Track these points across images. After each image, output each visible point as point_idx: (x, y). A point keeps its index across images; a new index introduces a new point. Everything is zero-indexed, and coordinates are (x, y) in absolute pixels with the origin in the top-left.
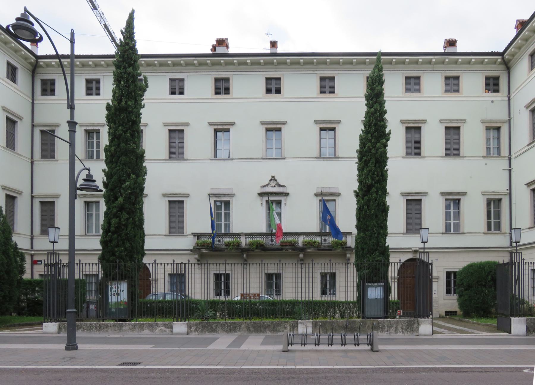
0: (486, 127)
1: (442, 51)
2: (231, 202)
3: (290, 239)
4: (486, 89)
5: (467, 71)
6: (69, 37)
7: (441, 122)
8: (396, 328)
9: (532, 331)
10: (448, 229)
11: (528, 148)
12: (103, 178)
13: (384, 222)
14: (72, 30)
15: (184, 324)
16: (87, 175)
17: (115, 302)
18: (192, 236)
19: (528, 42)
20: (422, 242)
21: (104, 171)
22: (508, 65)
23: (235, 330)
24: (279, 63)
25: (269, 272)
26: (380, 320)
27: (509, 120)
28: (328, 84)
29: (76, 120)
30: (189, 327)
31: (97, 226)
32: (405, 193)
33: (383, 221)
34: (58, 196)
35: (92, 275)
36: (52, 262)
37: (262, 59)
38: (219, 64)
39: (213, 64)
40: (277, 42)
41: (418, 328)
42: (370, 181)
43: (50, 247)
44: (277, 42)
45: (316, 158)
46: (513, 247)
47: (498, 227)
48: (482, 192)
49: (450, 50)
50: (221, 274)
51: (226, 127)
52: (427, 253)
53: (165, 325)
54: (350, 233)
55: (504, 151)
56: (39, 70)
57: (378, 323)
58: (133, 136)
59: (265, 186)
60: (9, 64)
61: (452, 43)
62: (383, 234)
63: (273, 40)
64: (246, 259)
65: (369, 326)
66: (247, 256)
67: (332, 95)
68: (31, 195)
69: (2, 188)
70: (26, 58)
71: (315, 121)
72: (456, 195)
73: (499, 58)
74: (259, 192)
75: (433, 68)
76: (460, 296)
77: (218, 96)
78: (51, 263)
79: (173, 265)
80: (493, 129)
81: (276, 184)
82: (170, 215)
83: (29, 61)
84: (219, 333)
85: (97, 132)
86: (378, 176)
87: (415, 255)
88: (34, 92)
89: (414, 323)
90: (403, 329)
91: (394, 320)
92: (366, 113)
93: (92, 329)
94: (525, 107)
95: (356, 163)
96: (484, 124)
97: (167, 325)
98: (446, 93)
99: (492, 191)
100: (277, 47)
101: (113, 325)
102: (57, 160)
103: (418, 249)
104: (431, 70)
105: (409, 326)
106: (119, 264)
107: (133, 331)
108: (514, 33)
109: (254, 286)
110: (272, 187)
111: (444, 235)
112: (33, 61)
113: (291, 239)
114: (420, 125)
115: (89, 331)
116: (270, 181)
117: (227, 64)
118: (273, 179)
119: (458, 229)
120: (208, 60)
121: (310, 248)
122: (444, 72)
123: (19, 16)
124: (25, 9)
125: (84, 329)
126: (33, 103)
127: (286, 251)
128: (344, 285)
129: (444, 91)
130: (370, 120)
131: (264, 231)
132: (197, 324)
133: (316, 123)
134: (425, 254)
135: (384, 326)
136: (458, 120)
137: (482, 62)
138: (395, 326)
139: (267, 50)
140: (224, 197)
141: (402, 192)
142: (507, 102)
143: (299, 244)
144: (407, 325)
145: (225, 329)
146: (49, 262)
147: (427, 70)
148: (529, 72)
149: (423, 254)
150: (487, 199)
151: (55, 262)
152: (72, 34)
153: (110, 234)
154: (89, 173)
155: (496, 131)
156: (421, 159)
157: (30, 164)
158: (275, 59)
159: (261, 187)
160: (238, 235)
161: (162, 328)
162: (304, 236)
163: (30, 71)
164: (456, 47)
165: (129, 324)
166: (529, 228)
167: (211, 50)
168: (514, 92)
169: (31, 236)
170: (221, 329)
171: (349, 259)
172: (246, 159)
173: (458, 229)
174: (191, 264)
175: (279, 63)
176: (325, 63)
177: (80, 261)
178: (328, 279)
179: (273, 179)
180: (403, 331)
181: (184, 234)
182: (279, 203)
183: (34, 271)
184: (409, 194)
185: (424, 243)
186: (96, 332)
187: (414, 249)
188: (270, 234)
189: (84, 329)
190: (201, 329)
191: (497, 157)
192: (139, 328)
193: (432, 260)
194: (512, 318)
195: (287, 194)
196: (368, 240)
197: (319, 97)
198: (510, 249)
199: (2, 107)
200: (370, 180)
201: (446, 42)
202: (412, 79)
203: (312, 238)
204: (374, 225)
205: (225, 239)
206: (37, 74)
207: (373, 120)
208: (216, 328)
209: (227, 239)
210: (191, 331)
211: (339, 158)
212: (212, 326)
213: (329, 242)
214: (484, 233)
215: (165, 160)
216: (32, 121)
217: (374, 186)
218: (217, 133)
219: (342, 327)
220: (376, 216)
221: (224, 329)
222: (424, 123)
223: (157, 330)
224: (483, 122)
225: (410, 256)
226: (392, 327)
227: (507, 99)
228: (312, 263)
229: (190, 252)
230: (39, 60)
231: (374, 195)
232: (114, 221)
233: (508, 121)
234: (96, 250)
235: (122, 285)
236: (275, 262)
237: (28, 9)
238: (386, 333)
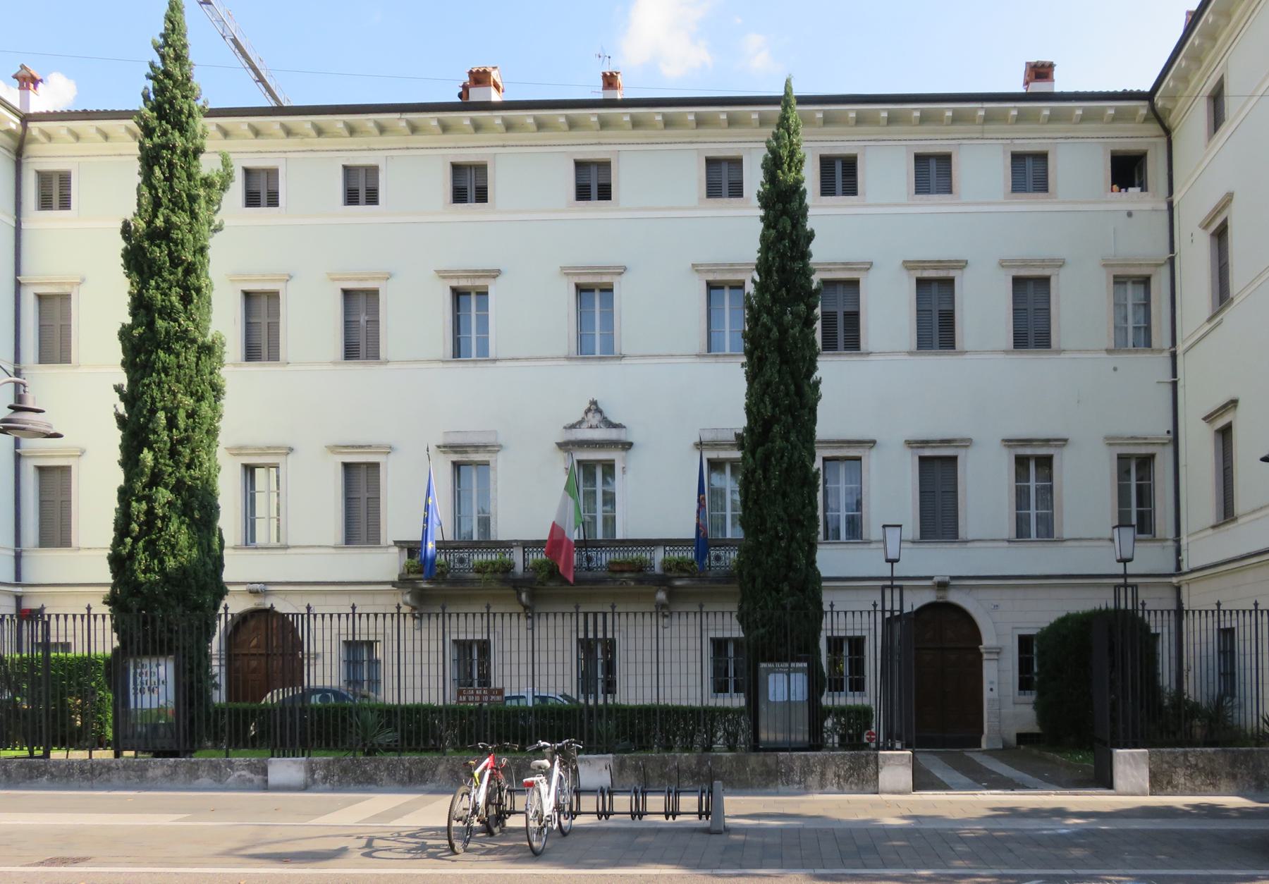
0: (1115, 277)
1: (1020, 89)
3: (634, 555)
4: (1113, 184)
5: (1066, 138)
7: (1003, 266)
8: (823, 774)
9: (1165, 782)
10: (1021, 532)
12: (115, 406)
13: (806, 510)
15: (295, 762)
17: (151, 708)
18: (396, 550)
20: (1119, 561)
21: (118, 389)
22: (1166, 125)
23: (421, 777)
25: (719, 635)
26: (781, 753)
30: (311, 771)
32: (916, 442)
33: (804, 507)
35: (362, 643)
41: (877, 773)
42: (768, 411)
48: (1106, 438)
49: (1039, 87)
50: (472, 642)
52: (1134, 587)
53: (249, 765)
55: (1160, 335)
56: (31, 149)
57: (777, 763)
58: (186, 300)
59: (573, 426)
61: (1040, 71)
62: (804, 541)
65: (753, 770)
68: (15, 452)
71: (693, 265)
72: (1043, 446)
74: (560, 440)
76: (1041, 695)
80: (1134, 283)
84: (381, 786)
86: (787, 394)
87: (941, 594)
89: (867, 763)
90: (839, 776)
91: (816, 756)
92: (761, 241)
93: (72, 775)
94: (1200, 226)
95: (743, 365)
97: (255, 764)
98: (1015, 194)
99: (1130, 435)
101: (124, 767)
103: (947, 579)
104: (977, 138)
105: (854, 770)
107: (172, 780)
110: (591, 427)
111: (1012, 545)
112: (13, 126)
113: (635, 554)
114: (951, 274)
115: (65, 781)
116: (586, 413)
118: (594, 407)
119: (1047, 531)
121: (680, 578)
122: (1009, 141)
125: (52, 774)
127: (622, 584)
128: (692, 670)
129: (1010, 189)
130: (768, 258)
132: (329, 763)
133: (697, 270)
134: (1129, 590)
135: (791, 770)
136: (476, 271)
138: (818, 769)
140: (477, 452)
141: (907, 439)
143: (653, 567)
144: (850, 768)
145: (397, 775)
147: (968, 139)
149: (1122, 590)
150: (1118, 455)
153: (128, 540)
155: (1141, 288)
159: (565, 428)
160: (507, 545)
161: (243, 773)
162: (667, 548)
163: (9, 151)
164: (1053, 81)
165: (162, 764)
166: (1214, 527)
170: (388, 775)
173: (1047, 531)
174: (838, 612)
177: (832, 606)
178: (731, 652)
179: (594, 407)
180: (839, 783)
181: (379, 544)
182: (609, 468)
184: (925, 443)
185: (1124, 561)
186: (82, 784)
187: (936, 579)
188: (583, 544)
189: (52, 774)
190: (338, 775)
192: (187, 772)
194: (1119, 752)
195: (627, 446)
196: (764, 557)
198: (1174, 580)
200: (769, 407)
201: (1028, 68)
202: (931, 161)
203: (639, 554)
204: (778, 516)
205: (476, 556)
206: (28, 157)
207: (774, 258)
208: (374, 774)
209: (480, 556)
210: (314, 781)
212: (365, 768)
216: (18, 271)
217: (778, 421)
219: (685, 771)
220: (785, 495)
221: (395, 775)
222: (962, 268)
223: (232, 778)
225: (929, 597)
226: (812, 772)
227: (1165, 206)
229: (389, 587)
231: (779, 443)
232: (138, 508)
233: (1168, 261)
235: (162, 669)
236: (628, 610)
238: (796, 786)
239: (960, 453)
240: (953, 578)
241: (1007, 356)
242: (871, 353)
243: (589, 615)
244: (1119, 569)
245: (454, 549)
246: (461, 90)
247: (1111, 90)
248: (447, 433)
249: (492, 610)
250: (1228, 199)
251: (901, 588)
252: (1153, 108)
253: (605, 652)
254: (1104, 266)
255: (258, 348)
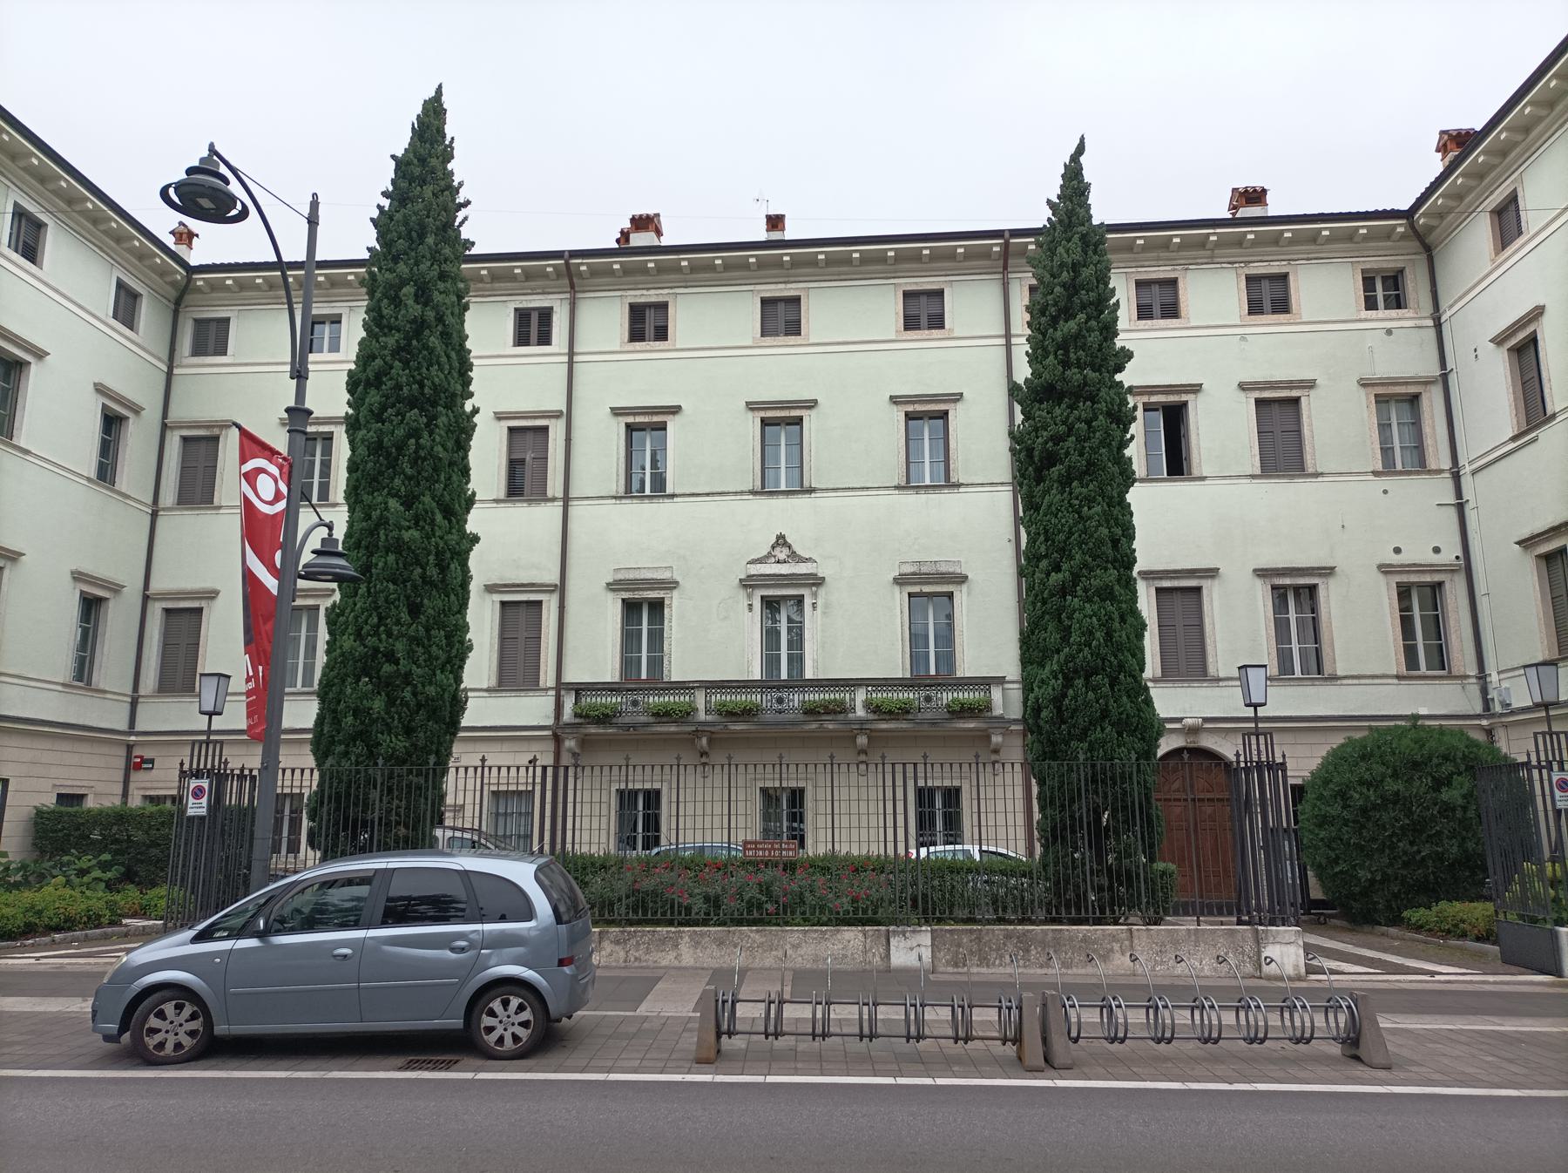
2: (667, 602)
5: (1308, 259)
6: (306, 211)
11: (1513, 445)
14: (314, 195)
16: (323, 540)
19: (1487, 181)
20: (1247, 705)
22: (1427, 241)
24: (797, 263)
27: (1445, 378)
28: (924, 308)
29: (308, 405)
31: (309, 669)
34: (212, 595)
36: (202, 766)
37: (752, 256)
38: (644, 271)
39: (627, 271)
40: (783, 216)
43: (201, 723)
44: (783, 216)
45: (897, 488)
46: (1493, 716)
47: (1440, 658)
50: (636, 792)
51: (656, 419)
52: (1268, 733)
54: (1000, 681)
55: (1438, 456)
56: (188, 298)
60: (121, 285)
61: (775, 222)
63: (772, 212)
64: (707, 749)
66: (710, 741)
67: (936, 333)
68: (144, 594)
69: (74, 578)
70: (163, 272)
73: (1400, 225)
75: (1212, 257)
77: (638, 345)
78: (198, 770)
79: (479, 770)
80: (1397, 401)
81: (788, 556)
82: (503, 639)
83: (169, 279)
85: (324, 439)
88: (174, 350)
96: (1370, 389)
100: (783, 229)
102: (220, 507)
106: (434, 770)
108: (1436, 165)
109: (708, 825)
112: (179, 277)
114: (1184, 398)
117: (661, 269)
118: (781, 541)
119: (1317, 668)
120: (616, 263)
123: (196, 163)
124: (212, 149)
126: (169, 375)
131: (756, 675)
136: (1291, 382)
137: (1351, 236)
139: (760, 234)
142: (1432, 333)
146: (195, 766)
148: (1497, 254)
151: (209, 766)
152: (315, 205)
154: (330, 535)
156: (1192, 483)
157: (148, 518)
158: (786, 255)
167: (618, 241)
168: (1451, 306)
169: (133, 699)
171: (996, 751)
172: (708, 495)
175: (797, 263)
176: (916, 257)
178: (939, 803)
179: (781, 541)
183: (132, 786)
191: (1418, 473)
193: (1284, 756)
197: (904, 338)
198: (1484, 722)
199: (95, 384)
211: (959, 485)
213: (940, 703)
214: (1398, 677)
215: (497, 501)
218: (634, 433)
224: (1365, 384)
228: (925, 764)
230: (195, 276)
234: (300, 729)
237: (217, 148)
239: (1206, 584)
240: (1206, 720)
241: (1253, 481)
242: (1322, 474)
243: (493, 769)
244: (1250, 712)
245: (611, 690)
246: (619, 236)
247: (232, 261)
248: (617, 570)
249: (631, 762)
250: (1538, 313)
251: (222, 742)
252: (1412, 225)
253: (647, 806)
254: (1364, 385)
255: (522, 488)
